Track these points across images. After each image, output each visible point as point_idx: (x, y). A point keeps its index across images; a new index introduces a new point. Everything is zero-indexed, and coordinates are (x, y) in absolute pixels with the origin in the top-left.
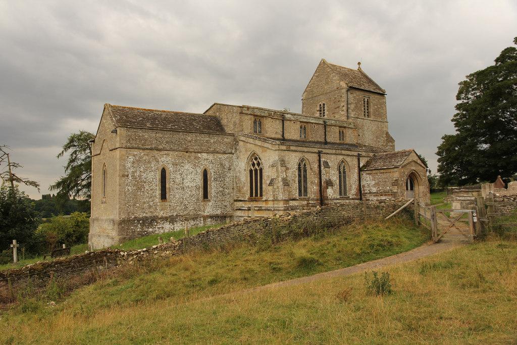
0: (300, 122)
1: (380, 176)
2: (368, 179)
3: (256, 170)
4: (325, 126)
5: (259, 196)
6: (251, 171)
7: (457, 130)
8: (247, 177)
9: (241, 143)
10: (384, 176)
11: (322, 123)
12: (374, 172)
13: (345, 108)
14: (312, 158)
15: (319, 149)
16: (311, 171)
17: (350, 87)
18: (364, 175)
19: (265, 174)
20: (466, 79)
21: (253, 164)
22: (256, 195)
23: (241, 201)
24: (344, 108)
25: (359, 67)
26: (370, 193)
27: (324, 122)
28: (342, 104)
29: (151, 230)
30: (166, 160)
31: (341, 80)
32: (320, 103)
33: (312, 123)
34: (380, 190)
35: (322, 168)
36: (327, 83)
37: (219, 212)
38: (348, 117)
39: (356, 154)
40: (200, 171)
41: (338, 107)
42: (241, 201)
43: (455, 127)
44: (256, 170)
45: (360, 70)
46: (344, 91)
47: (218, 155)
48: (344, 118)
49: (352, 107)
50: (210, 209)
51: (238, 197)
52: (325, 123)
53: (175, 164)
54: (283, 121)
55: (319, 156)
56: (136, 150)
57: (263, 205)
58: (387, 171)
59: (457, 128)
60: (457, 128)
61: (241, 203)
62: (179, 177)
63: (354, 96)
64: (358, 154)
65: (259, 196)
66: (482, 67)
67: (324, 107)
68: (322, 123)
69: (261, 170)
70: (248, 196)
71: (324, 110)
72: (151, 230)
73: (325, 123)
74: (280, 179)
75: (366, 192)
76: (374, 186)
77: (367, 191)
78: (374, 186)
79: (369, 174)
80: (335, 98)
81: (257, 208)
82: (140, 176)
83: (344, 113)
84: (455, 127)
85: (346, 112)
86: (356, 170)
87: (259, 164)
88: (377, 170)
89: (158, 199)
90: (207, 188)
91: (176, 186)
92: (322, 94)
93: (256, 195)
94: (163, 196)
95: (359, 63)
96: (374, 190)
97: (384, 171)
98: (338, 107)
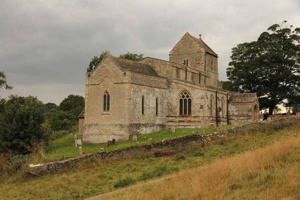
0: (192, 72)
1: (240, 106)
2: (232, 107)
3: (185, 100)
4: (200, 75)
5: (187, 114)
6: (181, 100)
7: (228, 79)
8: (178, 103)
9: (173, 84)
10: (242, 106)
11: (199, 73)
12: (236, 104)
13: (203, 65)
14: (214, 94)
15: (217, 90)
16: (213, 102)
17: (207, 52)
18: (230, 105)
19: (193, 103)
20: (237, 47)
21: (183, 97)
22: (185, 113)
23: (172, 116)
24: (203, 64)
25: (200, 38)
26: (233, 115)
27: (200, 73)
28: (202, 62)
29: (139, 131)
30: (144, 90)
31: (201, 47)
32: (185, 59)
33: (196, 73)
34: (240, 114)
35: (217, 100)
36: (190, 47)
37: (161, 123)
38: (205, 70)
39: (226, 93)
40: (155, 98)
41: (199, 63)
42: (172, 116)
43: (227, 76)
44: (185, 100)
45: (200, 39)
46: (204, 54)
47: (161, 89)
48: (203, 70)
49: (207, 64)
50: (158, 121)
51: (170, 115)
52: (186, 70)
53: (147, 94)
54: (186, 71)
55: (216, 94)
56: (134, 85)
57: (192, 119)
58: (244, 104)
59: (228, 77)
60: (228, 77)
61: (172, 118)
62: (148, 101)
63: (208, 57)
64: (227, 94)
65: (187, 114)
66: (249, 41)
67: (187, 62)
68: (199, 73)
69: (190, 101)
70: (178, 114)
71: (187, 64)
72: (139, 131)
73: (186, 70)
74: (206, 105)
75: (230, 114)
76: (236, 111)
77: (231, 114)
78: (236, 111)
79: (233, 105)
80: (196, 58)
81: (188, 121)
82: (135, 100)
83: (203, 67)
84: (227, 76)
85: (204, 67)
86: (226, 103)
87: (188, 96)
88: (239, 103)
89: (141, 114)
90: (180, 110)
91: (147, 106)
92: (187, 54)
93: (185, 113)
94: (143, 113)
95: (200, 35)
96: (236, 114)
97: (243, 104)
98: (199, 63)
